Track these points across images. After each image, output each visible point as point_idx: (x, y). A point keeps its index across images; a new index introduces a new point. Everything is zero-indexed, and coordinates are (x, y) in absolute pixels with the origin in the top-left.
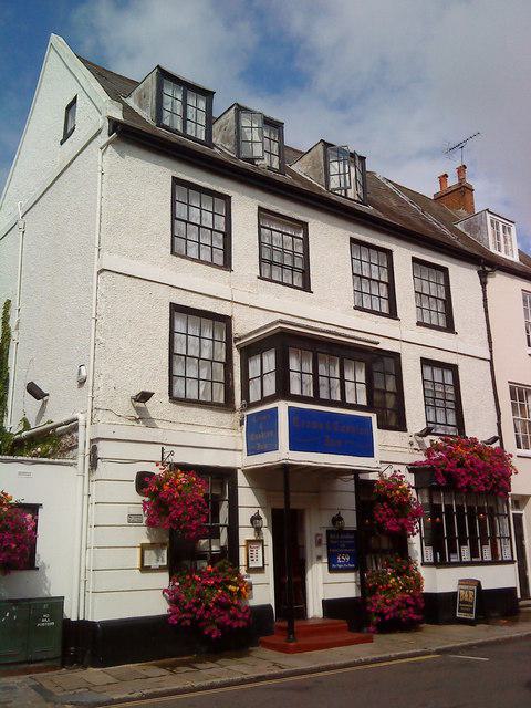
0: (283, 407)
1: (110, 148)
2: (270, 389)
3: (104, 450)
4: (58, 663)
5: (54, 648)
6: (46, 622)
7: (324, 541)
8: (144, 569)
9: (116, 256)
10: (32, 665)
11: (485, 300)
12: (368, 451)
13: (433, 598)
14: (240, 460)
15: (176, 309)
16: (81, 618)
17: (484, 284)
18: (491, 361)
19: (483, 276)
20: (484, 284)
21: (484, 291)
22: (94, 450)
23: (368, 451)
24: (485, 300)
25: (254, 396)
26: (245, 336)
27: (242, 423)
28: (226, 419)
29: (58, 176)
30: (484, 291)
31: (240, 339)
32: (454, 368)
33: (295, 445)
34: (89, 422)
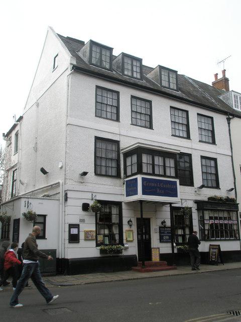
0: (139, 178)
11: (229, 130)
17: (229, 123)
18: (232, 157)
20: (229, 123)
21: (229, 126)
22: (66, 194)
24: (229, 130)
27: (124, 184)
30: (229, 126)
33: (144, 193)
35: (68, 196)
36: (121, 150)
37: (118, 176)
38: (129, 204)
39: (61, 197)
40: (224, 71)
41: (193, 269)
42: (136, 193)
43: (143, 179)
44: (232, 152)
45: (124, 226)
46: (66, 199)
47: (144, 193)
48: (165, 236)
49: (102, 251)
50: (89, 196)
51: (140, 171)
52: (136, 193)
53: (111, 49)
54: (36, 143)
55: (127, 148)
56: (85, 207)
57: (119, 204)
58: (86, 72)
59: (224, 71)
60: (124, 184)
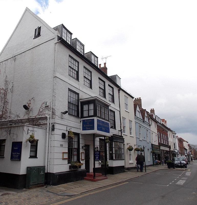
0: (96, 119)
1: (57, 44)
2: (92, 113)
3: (56, 126)
4: (43, 184)
5: (42, 180)
6: (42, 173)
7: (67, 137)
8: (63, 159)
9: (58, 73)
10: (38, 185)
11: (119, 97)
12: (109, 132)
13: (112, 168)
14: (81, 131)
15: (70, 90)
16: (48, 172)
17: (119, 93)
18: (120, 111)
19: (119, 91)
20: (119, 93)
21: (119, 94)
22: (53, 126)
23: (109, 132)
24: (119, 97)
25: (85, 114)
26: (83, 99)
27: (81, 122)
28: (78, 120)
29: (49, 40)
30: (119, 94)
31: (81, 99)
32: (114, 112)
33: (98, 129)
34: (51, 118)
35: (55, 127)
36: (80, 100)
37: (77, 116)
38: (83, 135)
39: (49, 127)
40: (105, 64)
41: (105, 176)
42: (93, 128)
43: (98, 121)
44: (120, 109)
45: (80, 149)
46: (53, 129)
47: (98, 129)
48: (97, 156)
49: (70, 167)
50: (65, 128)
51: (95, 115)
52: (93, 128)
53: (71, 34)
54: (13, 86)
55: (83, 99)
56: (64, 136)
57: (77, 135)
58: (64, 43)
59: (105, 64)
60: (81, 122)
